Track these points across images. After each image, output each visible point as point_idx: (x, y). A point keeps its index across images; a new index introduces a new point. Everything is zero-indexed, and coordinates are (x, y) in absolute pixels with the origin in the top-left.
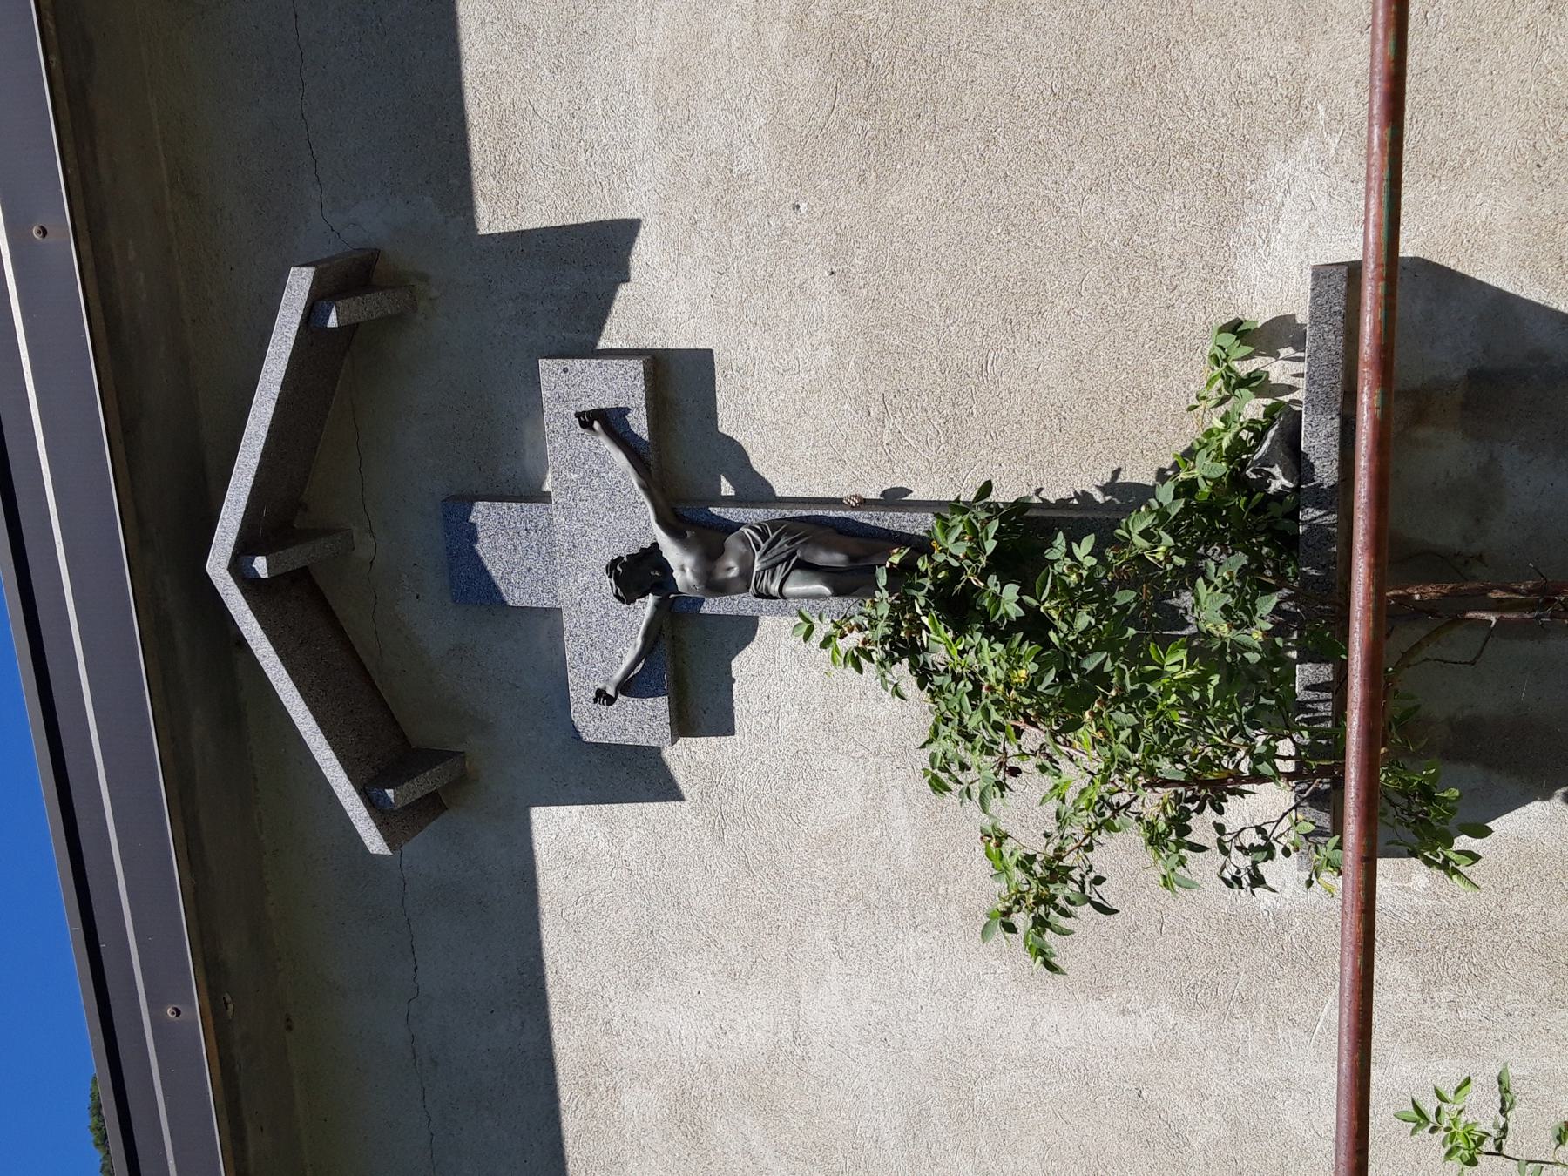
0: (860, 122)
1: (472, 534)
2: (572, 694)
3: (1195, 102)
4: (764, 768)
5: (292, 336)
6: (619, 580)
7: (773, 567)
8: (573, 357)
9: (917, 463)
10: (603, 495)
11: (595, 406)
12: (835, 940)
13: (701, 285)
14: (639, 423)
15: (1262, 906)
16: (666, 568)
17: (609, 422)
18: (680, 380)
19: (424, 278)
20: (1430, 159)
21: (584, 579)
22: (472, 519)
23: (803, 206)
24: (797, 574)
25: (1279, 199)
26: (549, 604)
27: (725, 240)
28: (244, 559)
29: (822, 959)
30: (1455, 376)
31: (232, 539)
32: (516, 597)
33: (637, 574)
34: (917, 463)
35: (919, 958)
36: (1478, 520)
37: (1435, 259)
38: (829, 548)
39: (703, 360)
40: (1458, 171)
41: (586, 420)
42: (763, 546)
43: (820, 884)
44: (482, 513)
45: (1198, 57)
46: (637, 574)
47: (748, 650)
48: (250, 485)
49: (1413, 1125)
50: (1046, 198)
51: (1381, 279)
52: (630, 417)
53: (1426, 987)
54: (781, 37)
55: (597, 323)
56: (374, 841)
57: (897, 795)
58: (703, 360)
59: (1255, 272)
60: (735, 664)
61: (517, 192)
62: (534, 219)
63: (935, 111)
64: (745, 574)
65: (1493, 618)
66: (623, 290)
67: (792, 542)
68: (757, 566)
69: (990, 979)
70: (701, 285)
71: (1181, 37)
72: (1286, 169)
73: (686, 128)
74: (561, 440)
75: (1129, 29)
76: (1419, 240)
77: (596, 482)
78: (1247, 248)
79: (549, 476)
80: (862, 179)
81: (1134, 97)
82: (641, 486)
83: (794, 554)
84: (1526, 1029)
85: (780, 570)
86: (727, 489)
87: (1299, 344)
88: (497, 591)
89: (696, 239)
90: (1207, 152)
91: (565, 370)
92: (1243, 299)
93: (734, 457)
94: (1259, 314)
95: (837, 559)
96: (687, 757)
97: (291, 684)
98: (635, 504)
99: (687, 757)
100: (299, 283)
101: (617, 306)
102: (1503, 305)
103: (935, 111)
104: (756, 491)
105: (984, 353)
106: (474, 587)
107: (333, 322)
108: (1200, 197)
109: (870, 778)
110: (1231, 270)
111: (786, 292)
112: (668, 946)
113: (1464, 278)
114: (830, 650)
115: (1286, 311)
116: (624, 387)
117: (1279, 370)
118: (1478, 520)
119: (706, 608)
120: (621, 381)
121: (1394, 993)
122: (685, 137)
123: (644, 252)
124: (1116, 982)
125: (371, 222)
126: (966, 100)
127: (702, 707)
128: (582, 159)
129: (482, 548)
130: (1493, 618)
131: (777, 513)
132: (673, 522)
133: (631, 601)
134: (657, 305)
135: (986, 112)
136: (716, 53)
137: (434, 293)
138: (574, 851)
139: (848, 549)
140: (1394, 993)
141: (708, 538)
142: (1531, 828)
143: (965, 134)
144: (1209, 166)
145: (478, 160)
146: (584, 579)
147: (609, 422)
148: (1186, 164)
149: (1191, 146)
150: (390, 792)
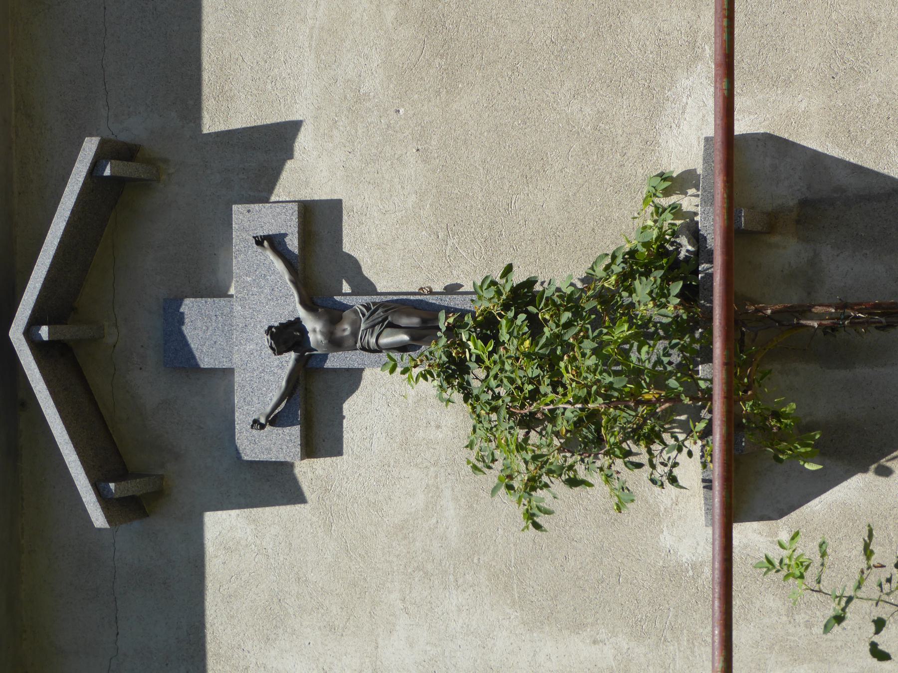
0: (438, 60)
1: (180, 319)
2: (237, 427)
3: (635, 46)
4: (361, 479)
5: (81, 180)
6: (273, 336)
7: (373, 327)
8: (253, 203)
9: (467, 268)
10: (267, 291)
11: (266, 233)
12: (403, 600)
13: (337, 160)
14: (293, 244)
15: (684, 560)
16: (304, 332)
17: (275, 243)
18: (320, 219)
19: (166, 161)
20: (770, 76)
21: (250, 347)
22: (181, 310)
23: (402, 111)
24: (388, 330)
25: (684, 100)
26: (226, 365)
27: (353, 132)
28: (34, 328)
29: (394, 615)
30: (791, 204)
31: (28, 312)
32: (205, 362)
33: (286, 337)
34: (467, 268)
35: (459, 610)
36: (809, 294)
37: (776, 134)
38: (409, 315)
39: (335, 207)
40: (788, 83)
41: (259, 242)
42: (367, 314)
43: (395, 559)
44: (189, 306)
45: (636, 21)
46: (286, 337)
47: (354, 395)
48: (44, 276)
49: (765, 570)
50: (548, 102)
51: (725, 17)
52: (287, 240)
53: (790, 613)
54: (393, 13)
55: (271, 190)
56: (98, 518)
57: (448, 493)
58: (335, 207)
59: (671, 144)
60: (345, 406)
61: (226, 109)
62: (237, 123)
63: (482, 53)
64: (355, 334)
65: (816, 325)
66: (289, 164)
67: (386, 311)
68: (363, 327)
69: (506, 623)
70: (337, 160)
71: (626, 9)
72: (688, 83)
73: (334, 67)
74: (242, 256)
75: (596, 5)
76: (767, 122)
77: (263, 283)
78: (667, 130)
79: (233, 285)
80: (438, 93)
81: (599, 43)
82: (291, 281)
83: (386, 318)
84: (856, 639)
85: (377, 329)
86: (346, 288)
87: (697, 187)
88: (194, 357)
89: (335, 132)
90: (642, 74)
91: (249, 211)
92: (665, 161)
93: (351, 268)
94: (676, 169)
95: (414, 321)
96: (309, 472)
97: (55, 410)
98: (287, 296)
99: (309, 472)
100: (90, 147)
101: (285, 175)
102: (817, 159)
103: (482, 53)
104: (364, 286)
105: (510, 196)
106: (179, 357)
107: (107, 172)
108: (638, 100)
109: (430, 482)
110: (658, 143)
111: (389, 162)
112: (291, 611)
113: (794, 144)
114: (407, 375)
115: (691, 167)
116: (287, 224)
117: (688, 202)
118: (809, 294)
119: (328, 364)
120: (283, 217)
121: (770, 617)
122: (332, 72)
123: (303, 141)
124: (590, 620)
125: (134, 128)
126: (501, 46)
127: (322, 440)
128: (269, 87)
129: (187, 330)
130: (816, 325)
131: (377, 299)
132: (309, 304)
133: (280, 353)
134: (308, 174)
135: (513, 53)
136: (354, 23)
137: (172, 170)
138: (231, 544)
139: (418, 321)
140: (770, 617)
141: (332, 314)
142: (855, 494)
143: (500, 66)
144: (643, 82)
145: (206, 90)
146: (250, 347)
147: (275, 243)
148: (630, 81)
149: (632, 70)
150: (112, 485)
